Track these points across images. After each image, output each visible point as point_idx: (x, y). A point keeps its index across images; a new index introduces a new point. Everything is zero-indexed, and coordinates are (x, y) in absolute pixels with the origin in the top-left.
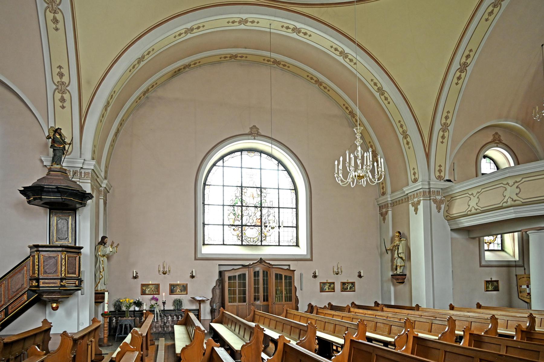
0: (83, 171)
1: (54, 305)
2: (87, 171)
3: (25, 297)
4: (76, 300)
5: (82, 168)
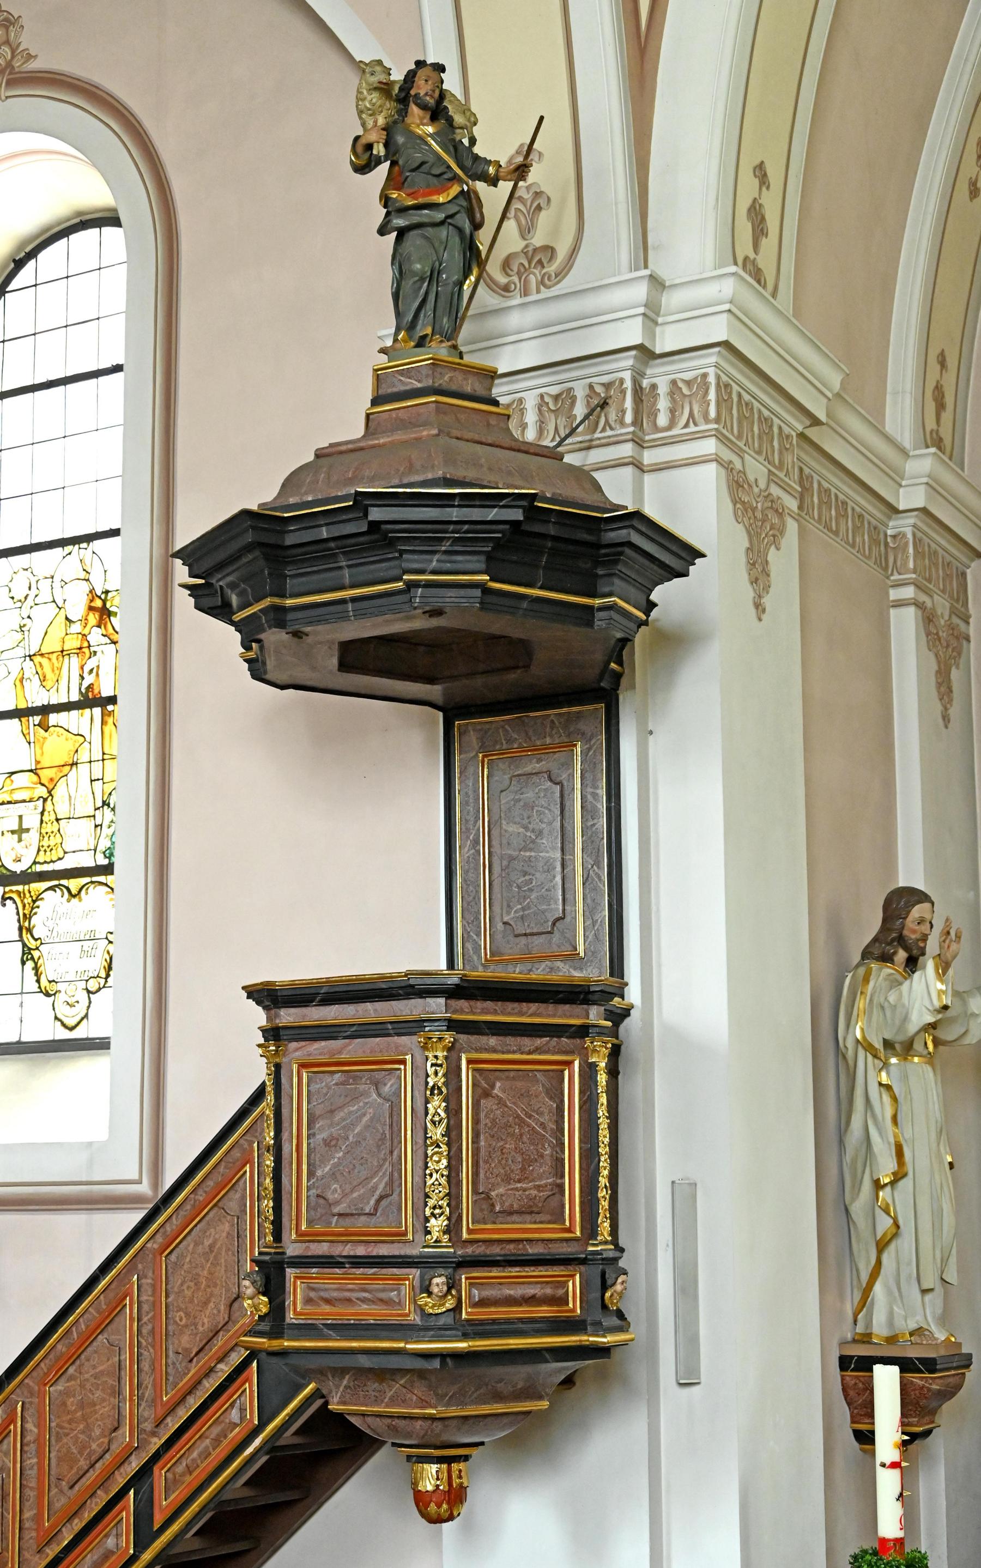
0: (660, 376)
1: (430, 1477)
2: (687, 369)
3: (246, 1402)
4: (638, 1427)
5: (645, 353)
